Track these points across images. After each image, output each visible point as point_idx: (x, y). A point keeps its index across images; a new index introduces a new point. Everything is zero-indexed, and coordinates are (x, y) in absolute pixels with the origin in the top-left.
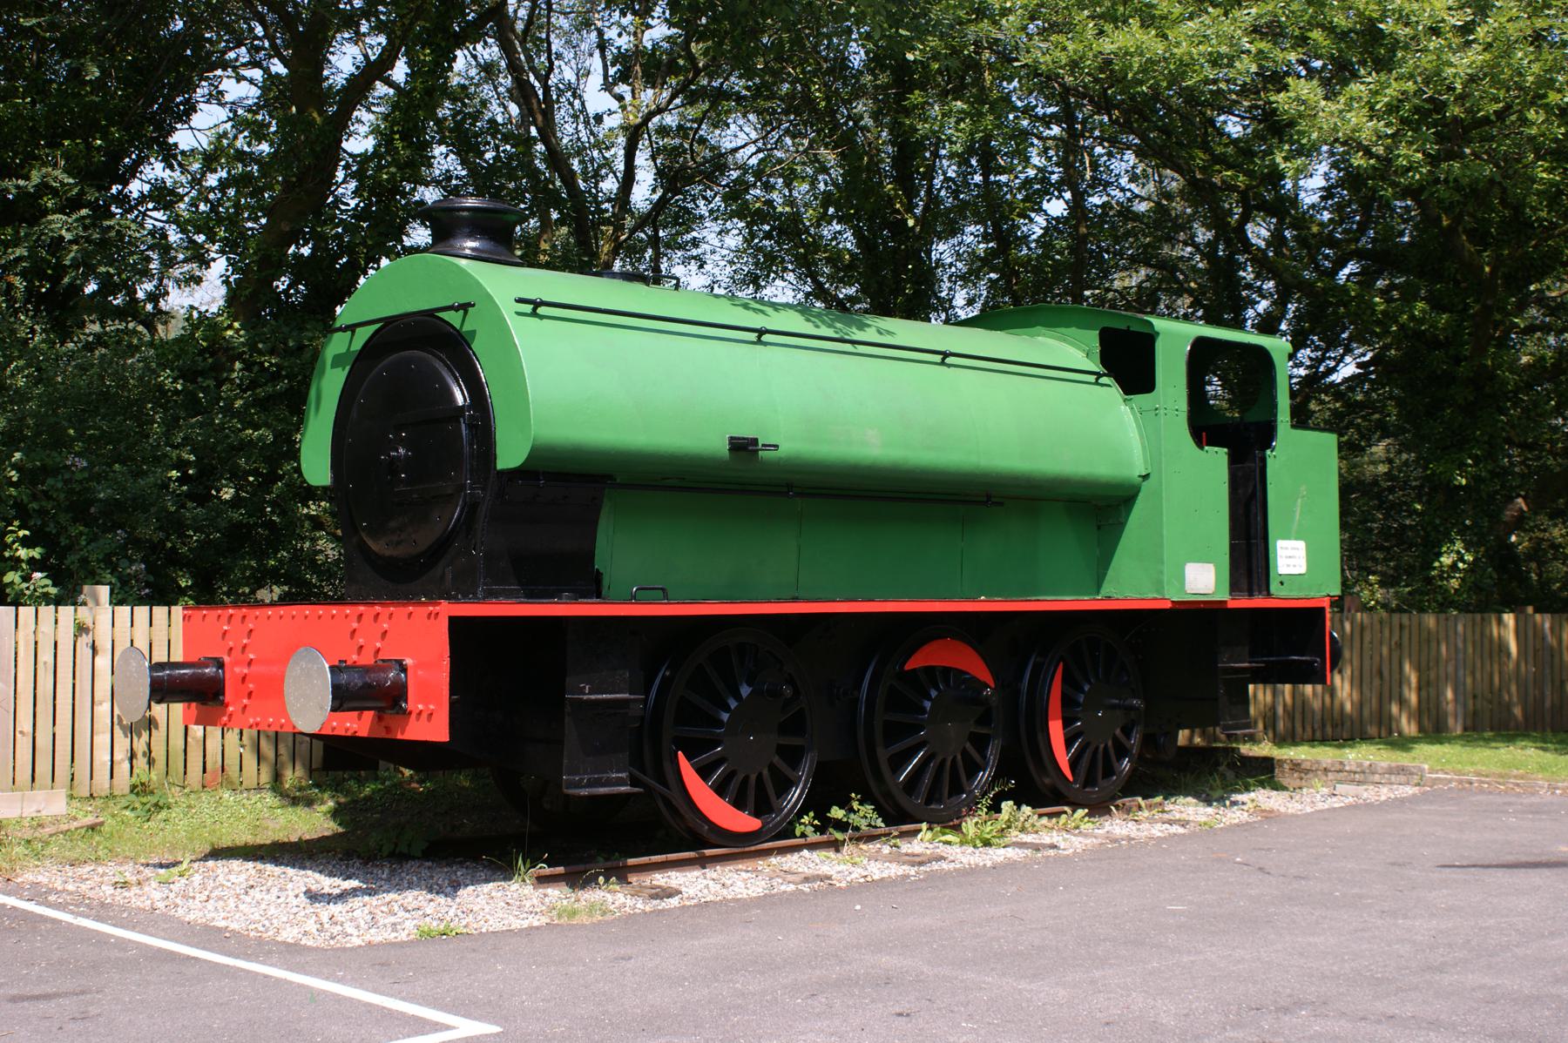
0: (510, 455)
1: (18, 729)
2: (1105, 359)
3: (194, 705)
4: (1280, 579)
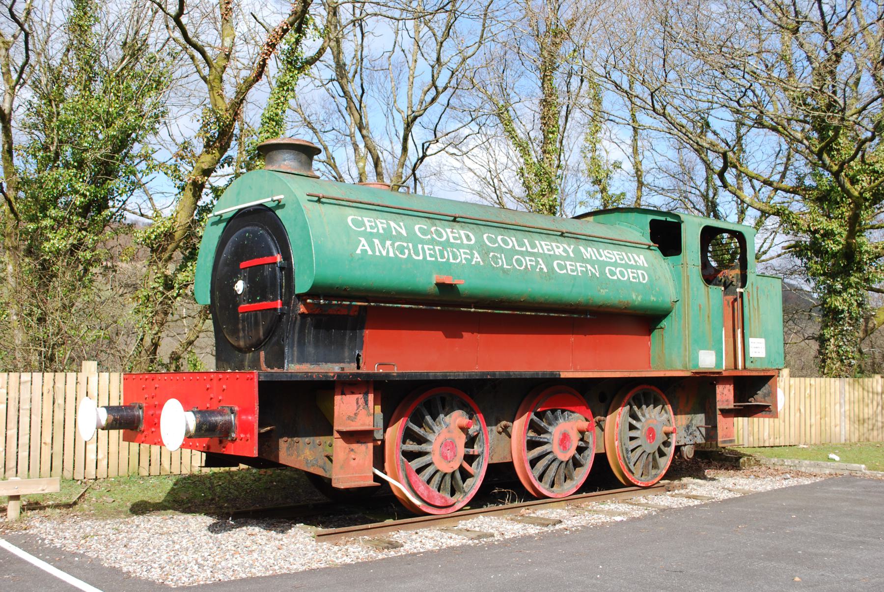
0: (302, 285)
1: (43, 441)
2: (653, 238)
3: (122, 431)
4: (752, 360)
